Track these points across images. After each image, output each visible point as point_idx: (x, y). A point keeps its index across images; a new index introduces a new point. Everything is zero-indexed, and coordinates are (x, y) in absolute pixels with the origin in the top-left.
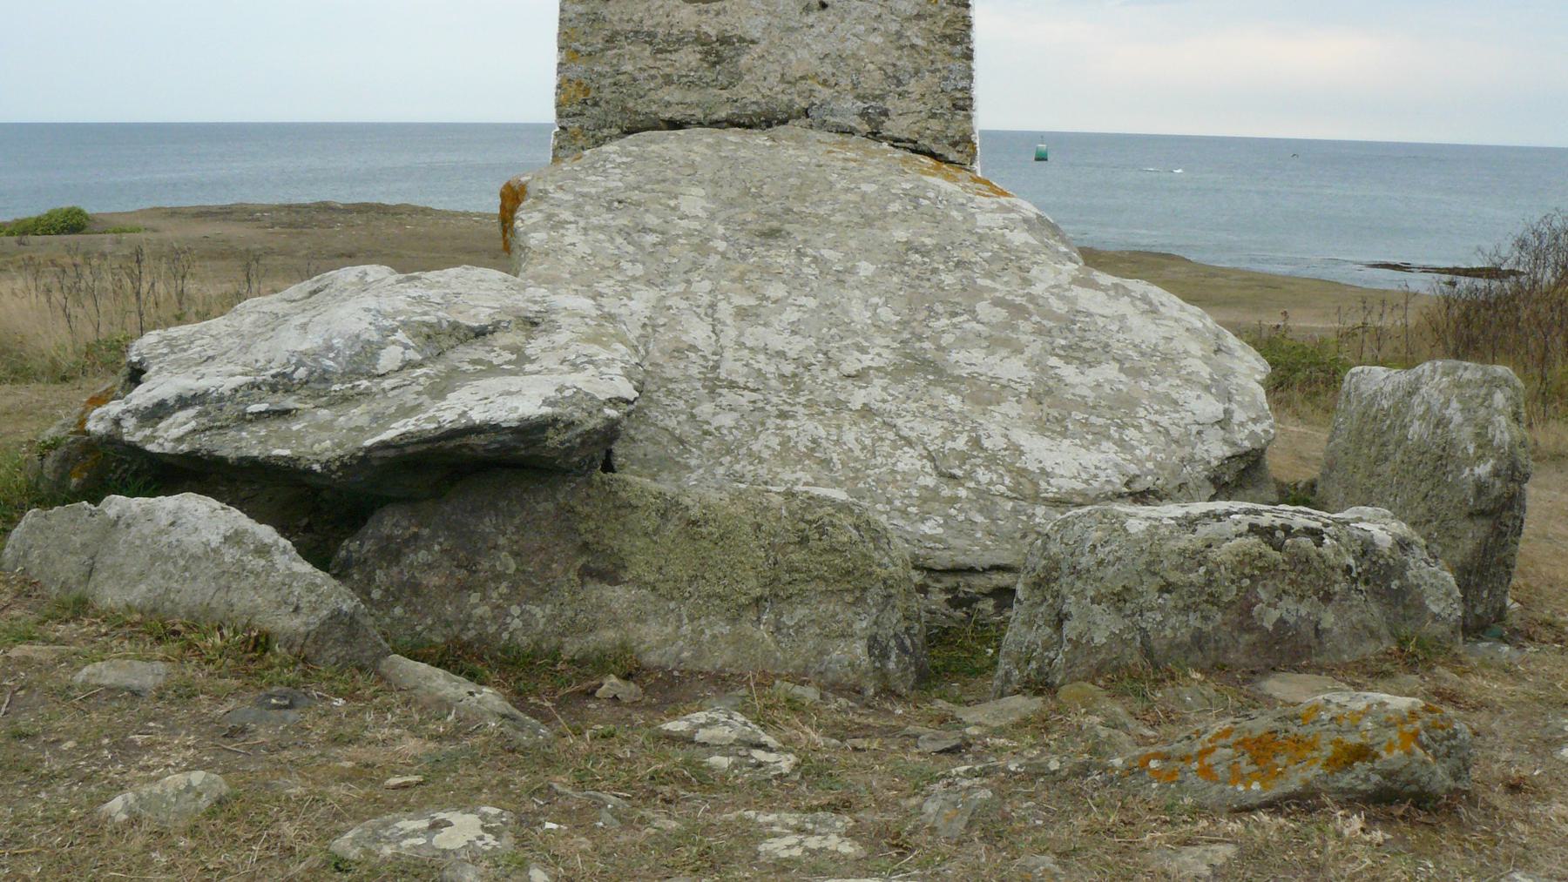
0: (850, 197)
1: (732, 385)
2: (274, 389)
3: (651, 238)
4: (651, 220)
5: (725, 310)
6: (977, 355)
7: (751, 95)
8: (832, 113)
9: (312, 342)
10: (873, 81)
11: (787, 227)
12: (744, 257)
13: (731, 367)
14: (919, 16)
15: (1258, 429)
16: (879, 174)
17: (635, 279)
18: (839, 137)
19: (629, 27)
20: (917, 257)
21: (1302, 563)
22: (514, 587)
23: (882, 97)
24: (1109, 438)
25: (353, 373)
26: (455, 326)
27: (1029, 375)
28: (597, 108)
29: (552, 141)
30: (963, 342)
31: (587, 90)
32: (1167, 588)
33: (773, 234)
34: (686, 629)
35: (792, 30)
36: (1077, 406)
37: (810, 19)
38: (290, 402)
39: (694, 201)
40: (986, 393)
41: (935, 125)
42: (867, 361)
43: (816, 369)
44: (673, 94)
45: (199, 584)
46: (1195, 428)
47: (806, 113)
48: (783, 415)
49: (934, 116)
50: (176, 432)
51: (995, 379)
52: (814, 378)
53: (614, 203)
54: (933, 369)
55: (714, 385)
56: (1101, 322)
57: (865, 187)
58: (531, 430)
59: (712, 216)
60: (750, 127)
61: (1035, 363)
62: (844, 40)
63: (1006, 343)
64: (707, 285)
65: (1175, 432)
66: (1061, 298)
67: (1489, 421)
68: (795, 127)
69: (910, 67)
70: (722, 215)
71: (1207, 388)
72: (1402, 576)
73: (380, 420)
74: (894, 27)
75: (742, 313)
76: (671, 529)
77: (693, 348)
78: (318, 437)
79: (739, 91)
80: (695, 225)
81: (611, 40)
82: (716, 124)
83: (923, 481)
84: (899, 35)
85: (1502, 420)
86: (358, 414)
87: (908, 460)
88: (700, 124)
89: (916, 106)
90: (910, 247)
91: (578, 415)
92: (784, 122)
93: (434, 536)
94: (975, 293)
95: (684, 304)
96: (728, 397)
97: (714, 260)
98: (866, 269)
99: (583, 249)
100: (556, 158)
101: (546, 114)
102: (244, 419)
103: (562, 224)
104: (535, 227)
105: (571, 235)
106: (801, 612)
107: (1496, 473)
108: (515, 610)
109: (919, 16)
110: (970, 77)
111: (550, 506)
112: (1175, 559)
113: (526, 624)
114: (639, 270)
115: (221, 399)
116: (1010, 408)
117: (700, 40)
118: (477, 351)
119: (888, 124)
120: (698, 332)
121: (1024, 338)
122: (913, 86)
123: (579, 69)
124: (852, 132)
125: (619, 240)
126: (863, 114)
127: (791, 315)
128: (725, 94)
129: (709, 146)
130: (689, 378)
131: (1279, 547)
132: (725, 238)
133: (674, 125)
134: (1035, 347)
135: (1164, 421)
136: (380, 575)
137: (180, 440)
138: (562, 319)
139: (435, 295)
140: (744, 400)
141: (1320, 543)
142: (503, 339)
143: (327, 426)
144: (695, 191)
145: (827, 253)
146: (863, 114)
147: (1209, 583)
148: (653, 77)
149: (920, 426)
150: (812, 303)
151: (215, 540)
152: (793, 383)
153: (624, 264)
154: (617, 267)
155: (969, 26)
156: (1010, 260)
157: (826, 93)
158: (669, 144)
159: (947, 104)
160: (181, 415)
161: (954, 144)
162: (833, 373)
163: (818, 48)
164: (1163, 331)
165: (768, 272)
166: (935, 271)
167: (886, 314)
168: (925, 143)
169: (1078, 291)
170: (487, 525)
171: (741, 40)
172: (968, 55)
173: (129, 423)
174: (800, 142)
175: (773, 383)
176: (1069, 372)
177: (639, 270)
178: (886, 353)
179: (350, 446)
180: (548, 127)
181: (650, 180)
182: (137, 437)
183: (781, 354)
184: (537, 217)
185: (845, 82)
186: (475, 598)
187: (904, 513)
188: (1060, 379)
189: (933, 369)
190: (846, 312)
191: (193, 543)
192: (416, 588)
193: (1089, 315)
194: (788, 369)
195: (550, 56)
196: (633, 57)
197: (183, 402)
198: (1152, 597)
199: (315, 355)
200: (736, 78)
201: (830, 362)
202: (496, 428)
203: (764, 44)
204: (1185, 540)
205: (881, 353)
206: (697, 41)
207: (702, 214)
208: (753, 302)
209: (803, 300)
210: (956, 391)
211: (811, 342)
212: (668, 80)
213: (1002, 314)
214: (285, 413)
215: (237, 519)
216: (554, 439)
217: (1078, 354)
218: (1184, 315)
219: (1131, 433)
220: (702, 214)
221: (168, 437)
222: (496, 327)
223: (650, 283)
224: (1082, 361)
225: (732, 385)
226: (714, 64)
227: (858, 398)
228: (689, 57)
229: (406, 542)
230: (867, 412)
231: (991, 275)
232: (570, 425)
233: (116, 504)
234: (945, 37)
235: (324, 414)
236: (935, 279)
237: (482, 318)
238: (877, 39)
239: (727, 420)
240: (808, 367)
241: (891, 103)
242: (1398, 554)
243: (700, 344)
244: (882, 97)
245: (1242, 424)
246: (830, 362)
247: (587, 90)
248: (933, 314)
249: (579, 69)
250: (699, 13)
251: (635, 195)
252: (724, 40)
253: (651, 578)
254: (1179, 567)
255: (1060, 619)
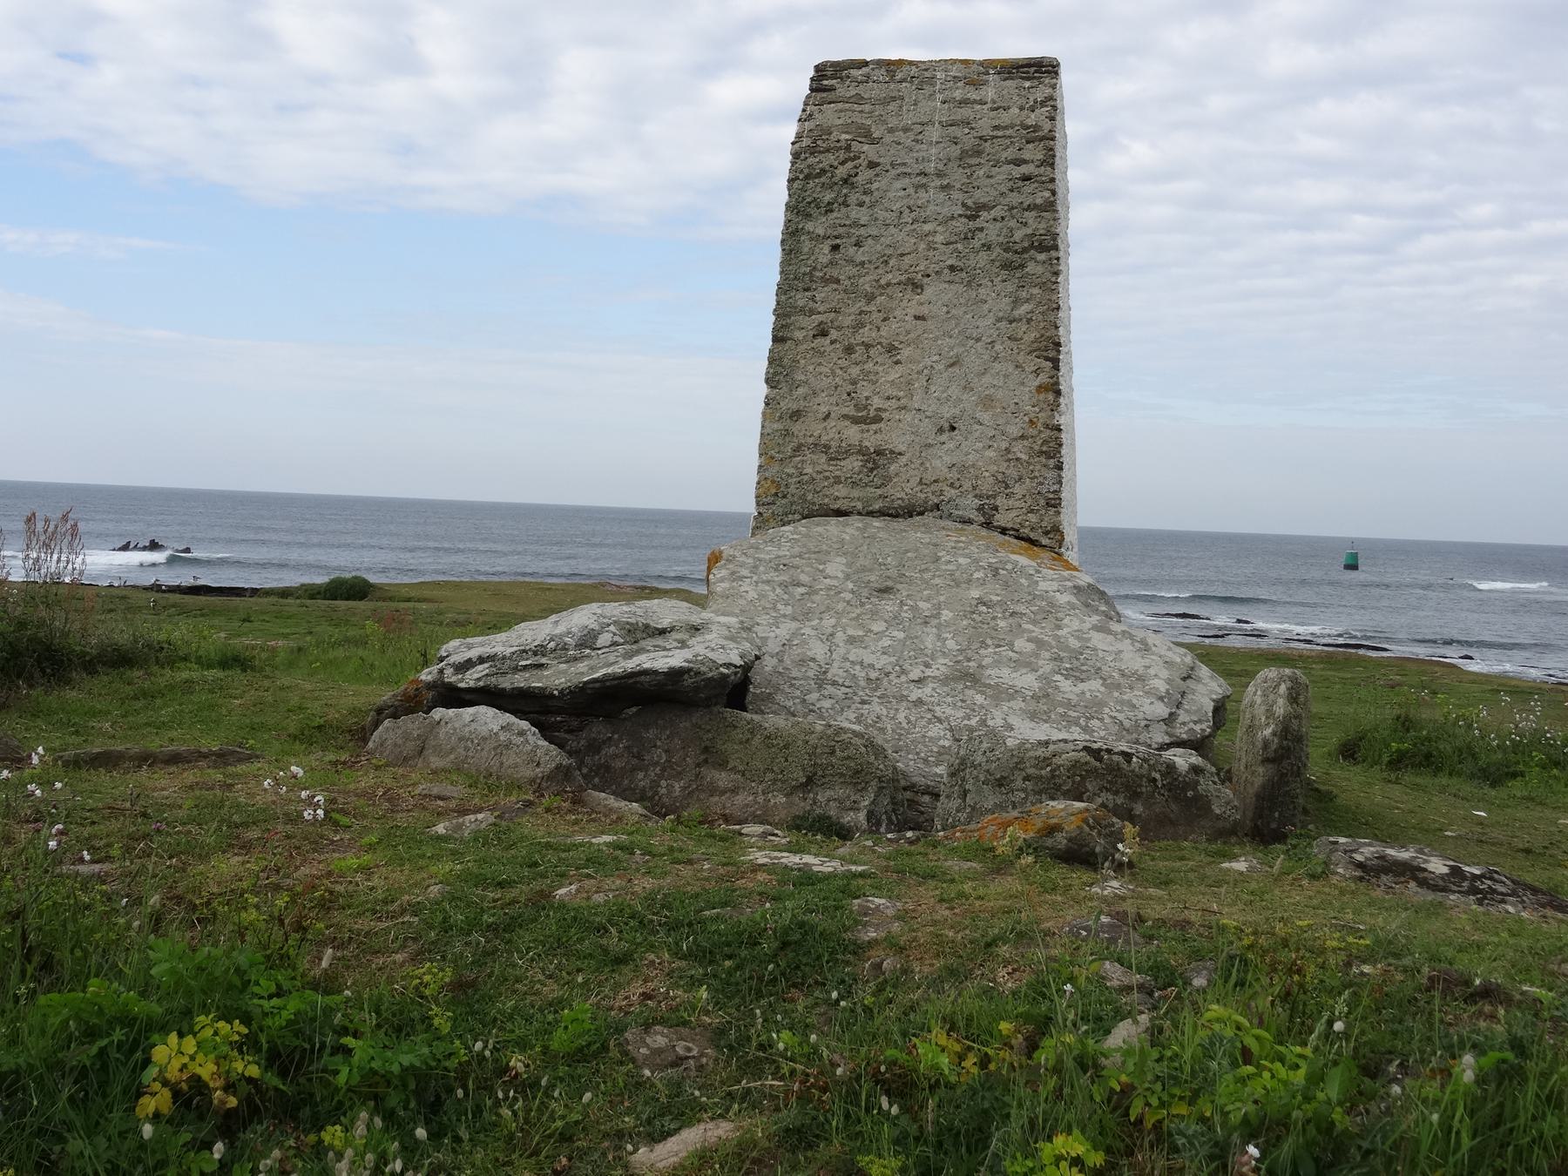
0: (950, 567)
1: (834, 683)
2: (535, 654)
3: (801, 590)
4: (804, 578)
5: (840, 637)
6: (1005, 672)
7: (903, 489)
8: (957, 507)
9: (560, 629)
10: (986, 486)
11: (899, 586)
12: (862, 605)
13: (835, 672)
14: (1022, 437)
15: (1197, 728)
16: (968, 552)
17: (784, 616)
18: (959, 526)
19: (811, 440)
20: (984, 609)
21: (1114, 770)
22: (663, 770)
23: (994, 496)
24: (1077, 724)
25: (581, 645)
26: (647, 626)
27: (1036, 685)
28: (786, 496)
29: (752, 523)
30: (997, 663)
31: (779, 486)
32: (1027, 778)
33: (886, 590)
34: (761, 799)
35: (930, 446)
36: (1061, 704)
37: (944, 437)
38: (544, 660)
39: (836, 567)
40: (1001, 694)
41: (1033, 518)
42: (928, 672)
43: (892, 677)
44: (841, 491)
45: (485, 753)
46: (1143, 723)
47: (937, 507)
48: (863, 702)
49: (1032, 511)
50: (476, 676)
51: (1012, 687)
52: (890, 682)
53: (781, 565)
54: (972, 679)
55: (821, 681)
56: (1101, 654)
57: (961, 560)
58: (676, 674)
59: (847, 577)
60: (897, 516)
61: (1045, 679)
62: (968, 454)
63: (1028, 665)
64: (833, 621)
65: (1127, 724)
66: (1078, 638)
67: (1275, 702)
68: (928, 518)
69: (1015, 475)
70: (855, 577)
71: (1161, 699)
72: (1195, 789)
73: (592, 669)
74: (1004, 445)
75: (851, 640)
76: (757, 741)
77: (813, 660)
78: (557, 677)
79: (889, 490)
80: (835, 582)
81: (798, 449)
82: (871, 514)
83: (941, 743)
84: (1007, 450)
85: (1281, 701)
86: (582, 666)
87: (935, 730)
88: (860, 514)
89: (1017, 504)
90: (981, 602)
91: (703, 669)
92: (921, 513)
93: (620, 739)
94: (1017, 630)
95: (813, 633)
96: (830, 689)
97: (840, 606)
98: (947, 615)
99: (752, 595)
100: (753, 534)
101: (749, 507)
102: (516, 669)
103: (742, 578)
104: (722, 580)
105: (746, 586)
106: (829, 793)
107: (1274, 734)
108: (663, 783)
109: (1022, 437)
110: (1060, 483)
111: (688, 724)
112: (1033, 762)
113: (669, 792)
114: (789, 610)
115: (504, 658)
116: (1018, 704)
117: (862, 451)
118: (659, 641)
119: (997, 516)
120: (818, 650)
121: (1041, 663)
122: (1018, 490)
123: (774, 469)
124: (970, 522)
125: (778, 590)
126: (980, 509)
127: (886, 642)
128: (879, 492)
129: (858, 529)
130: (806, 678)
131: (1100, 760)
132: (853, 592)
133: (839, 513)
134: (1047, 667)
135: (1121, 716)
136: (588, 760)
137: (479, 679)
138: (714, 628)
139: (640, 612)
140: (839, 693)
141: (1129, 762)
142: (675, 635)
143: (565, 672)
144: (838, 559)
145: (921, 604)
146: (980, 509)
147: (1053, 777)
148: (827, 478)
149: (949, 711)
150: (901, 635)
151: (496, 728)
152: (874, 684)
153: (779, 606)
154: (774, 608)
155: (1061, 445)
156: (1050, 611)
157: (951, 493)
158: (833, 526)
159: (1042, 502)
160: (480, 667)
161: (1046, 533)
162: (903, 678)
163: (948, 459)
164: (1147, 662)
165: (874, 614)
166: (994, 618)
167: (951, 644)
168: (1025, 531)
169: (1094, 634)
170: (651, 734)
171: (892, 452)
172: (1059, 467)
173: (449, 671)
174: (927, 529)
175: (862, 683)
176: (1065, 685)
177: (789, 610)
178: (943, 668)
179: (575, 681)
180: (744, 516)
181: (809, 552)
182: (453, 679)
183: (872, 666)
184: (724, 573)
185: (967, 485)
186: (641, 775)
187: (926, 761)
188: (1057, 688)
189: (972, 679)
190: (922, 642)
191: (484, 731)
192: (608, 768)
193: (1095, 649)
194: (873, 675)
195: (754, 460)
196: (813, 463)
197: (481, 660)
198: (1019, 783)
199: (561, 636)
200: (887, 480)
201: (904, 672)
202: (655, 672)
203: (908, 455)
204: (1040, 752)
205: (940, 667)
206: (860, 452)
207: (840, 575)
208: (861, 633)
209: (896, 633)
210: (982, 693)
211: (893, 659)
212: (837, 481)
213: (1030, 647)
214: (540, 666)
215: (509, 718)
216: (688, 681)
217: (1077, 675)
218: (1170, 654)
219: (1095, 723)
220: (840, 575)
221: (470, 679)
222: (672, 629)
223: (794, 619)
224: (1077, 678)
225: (834, 683)
226: (872, 470)
227: (915, 694)
228: (853, 464)
229: (604, 742)
230: (919, 702)
231: (1034, 622)
232: (698, 673)
233: (438, 713)
234: (1042, 452)
235: (563, 666)
236: (992, 624)
237: (665, 623)
238: (991, 453)
239: (827, 704)
240: (887, 674)
241: (1000, 501)
242: (1192, 776)
243: (818, 657)
244: (994, 496)
245: (1184, 724)
246: (904, 672)
247: (779, 486)
248: (984, 645)
249: (774, 469)
250: (862, 431)
251: (797, 561)
252: (879, 453)
253: (741, 768)
254: (1035, 766)
255: (965, 793)
